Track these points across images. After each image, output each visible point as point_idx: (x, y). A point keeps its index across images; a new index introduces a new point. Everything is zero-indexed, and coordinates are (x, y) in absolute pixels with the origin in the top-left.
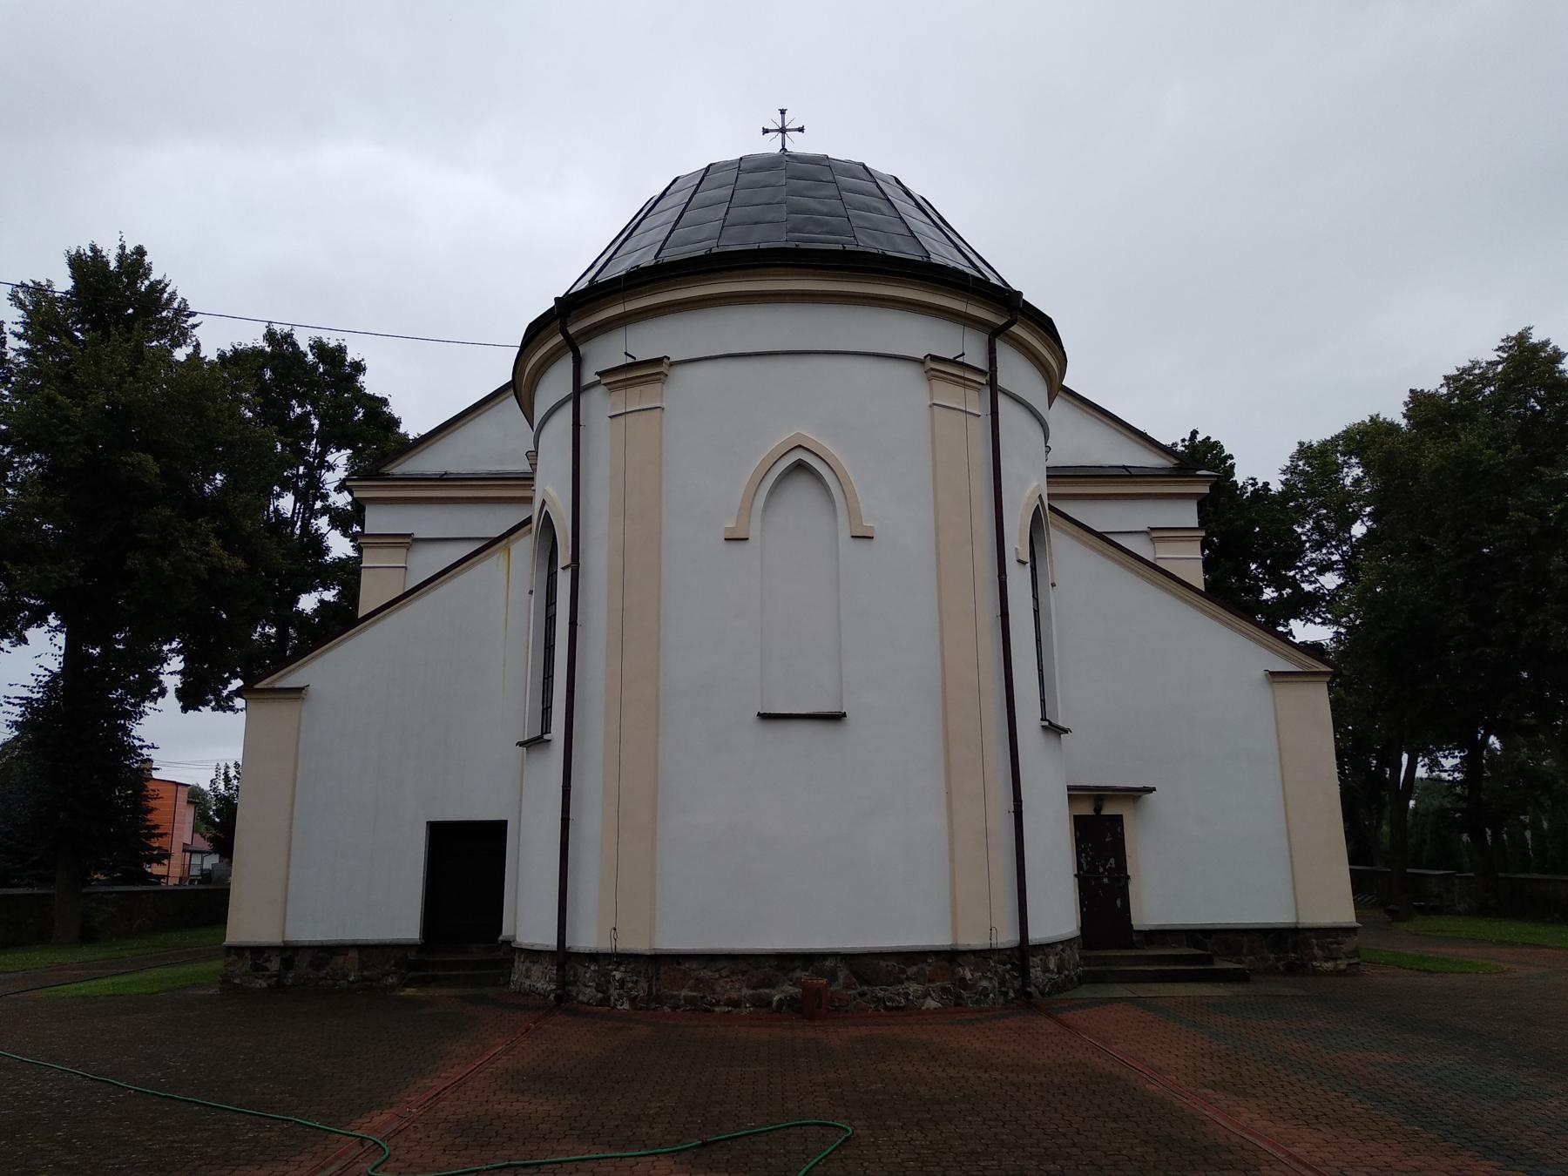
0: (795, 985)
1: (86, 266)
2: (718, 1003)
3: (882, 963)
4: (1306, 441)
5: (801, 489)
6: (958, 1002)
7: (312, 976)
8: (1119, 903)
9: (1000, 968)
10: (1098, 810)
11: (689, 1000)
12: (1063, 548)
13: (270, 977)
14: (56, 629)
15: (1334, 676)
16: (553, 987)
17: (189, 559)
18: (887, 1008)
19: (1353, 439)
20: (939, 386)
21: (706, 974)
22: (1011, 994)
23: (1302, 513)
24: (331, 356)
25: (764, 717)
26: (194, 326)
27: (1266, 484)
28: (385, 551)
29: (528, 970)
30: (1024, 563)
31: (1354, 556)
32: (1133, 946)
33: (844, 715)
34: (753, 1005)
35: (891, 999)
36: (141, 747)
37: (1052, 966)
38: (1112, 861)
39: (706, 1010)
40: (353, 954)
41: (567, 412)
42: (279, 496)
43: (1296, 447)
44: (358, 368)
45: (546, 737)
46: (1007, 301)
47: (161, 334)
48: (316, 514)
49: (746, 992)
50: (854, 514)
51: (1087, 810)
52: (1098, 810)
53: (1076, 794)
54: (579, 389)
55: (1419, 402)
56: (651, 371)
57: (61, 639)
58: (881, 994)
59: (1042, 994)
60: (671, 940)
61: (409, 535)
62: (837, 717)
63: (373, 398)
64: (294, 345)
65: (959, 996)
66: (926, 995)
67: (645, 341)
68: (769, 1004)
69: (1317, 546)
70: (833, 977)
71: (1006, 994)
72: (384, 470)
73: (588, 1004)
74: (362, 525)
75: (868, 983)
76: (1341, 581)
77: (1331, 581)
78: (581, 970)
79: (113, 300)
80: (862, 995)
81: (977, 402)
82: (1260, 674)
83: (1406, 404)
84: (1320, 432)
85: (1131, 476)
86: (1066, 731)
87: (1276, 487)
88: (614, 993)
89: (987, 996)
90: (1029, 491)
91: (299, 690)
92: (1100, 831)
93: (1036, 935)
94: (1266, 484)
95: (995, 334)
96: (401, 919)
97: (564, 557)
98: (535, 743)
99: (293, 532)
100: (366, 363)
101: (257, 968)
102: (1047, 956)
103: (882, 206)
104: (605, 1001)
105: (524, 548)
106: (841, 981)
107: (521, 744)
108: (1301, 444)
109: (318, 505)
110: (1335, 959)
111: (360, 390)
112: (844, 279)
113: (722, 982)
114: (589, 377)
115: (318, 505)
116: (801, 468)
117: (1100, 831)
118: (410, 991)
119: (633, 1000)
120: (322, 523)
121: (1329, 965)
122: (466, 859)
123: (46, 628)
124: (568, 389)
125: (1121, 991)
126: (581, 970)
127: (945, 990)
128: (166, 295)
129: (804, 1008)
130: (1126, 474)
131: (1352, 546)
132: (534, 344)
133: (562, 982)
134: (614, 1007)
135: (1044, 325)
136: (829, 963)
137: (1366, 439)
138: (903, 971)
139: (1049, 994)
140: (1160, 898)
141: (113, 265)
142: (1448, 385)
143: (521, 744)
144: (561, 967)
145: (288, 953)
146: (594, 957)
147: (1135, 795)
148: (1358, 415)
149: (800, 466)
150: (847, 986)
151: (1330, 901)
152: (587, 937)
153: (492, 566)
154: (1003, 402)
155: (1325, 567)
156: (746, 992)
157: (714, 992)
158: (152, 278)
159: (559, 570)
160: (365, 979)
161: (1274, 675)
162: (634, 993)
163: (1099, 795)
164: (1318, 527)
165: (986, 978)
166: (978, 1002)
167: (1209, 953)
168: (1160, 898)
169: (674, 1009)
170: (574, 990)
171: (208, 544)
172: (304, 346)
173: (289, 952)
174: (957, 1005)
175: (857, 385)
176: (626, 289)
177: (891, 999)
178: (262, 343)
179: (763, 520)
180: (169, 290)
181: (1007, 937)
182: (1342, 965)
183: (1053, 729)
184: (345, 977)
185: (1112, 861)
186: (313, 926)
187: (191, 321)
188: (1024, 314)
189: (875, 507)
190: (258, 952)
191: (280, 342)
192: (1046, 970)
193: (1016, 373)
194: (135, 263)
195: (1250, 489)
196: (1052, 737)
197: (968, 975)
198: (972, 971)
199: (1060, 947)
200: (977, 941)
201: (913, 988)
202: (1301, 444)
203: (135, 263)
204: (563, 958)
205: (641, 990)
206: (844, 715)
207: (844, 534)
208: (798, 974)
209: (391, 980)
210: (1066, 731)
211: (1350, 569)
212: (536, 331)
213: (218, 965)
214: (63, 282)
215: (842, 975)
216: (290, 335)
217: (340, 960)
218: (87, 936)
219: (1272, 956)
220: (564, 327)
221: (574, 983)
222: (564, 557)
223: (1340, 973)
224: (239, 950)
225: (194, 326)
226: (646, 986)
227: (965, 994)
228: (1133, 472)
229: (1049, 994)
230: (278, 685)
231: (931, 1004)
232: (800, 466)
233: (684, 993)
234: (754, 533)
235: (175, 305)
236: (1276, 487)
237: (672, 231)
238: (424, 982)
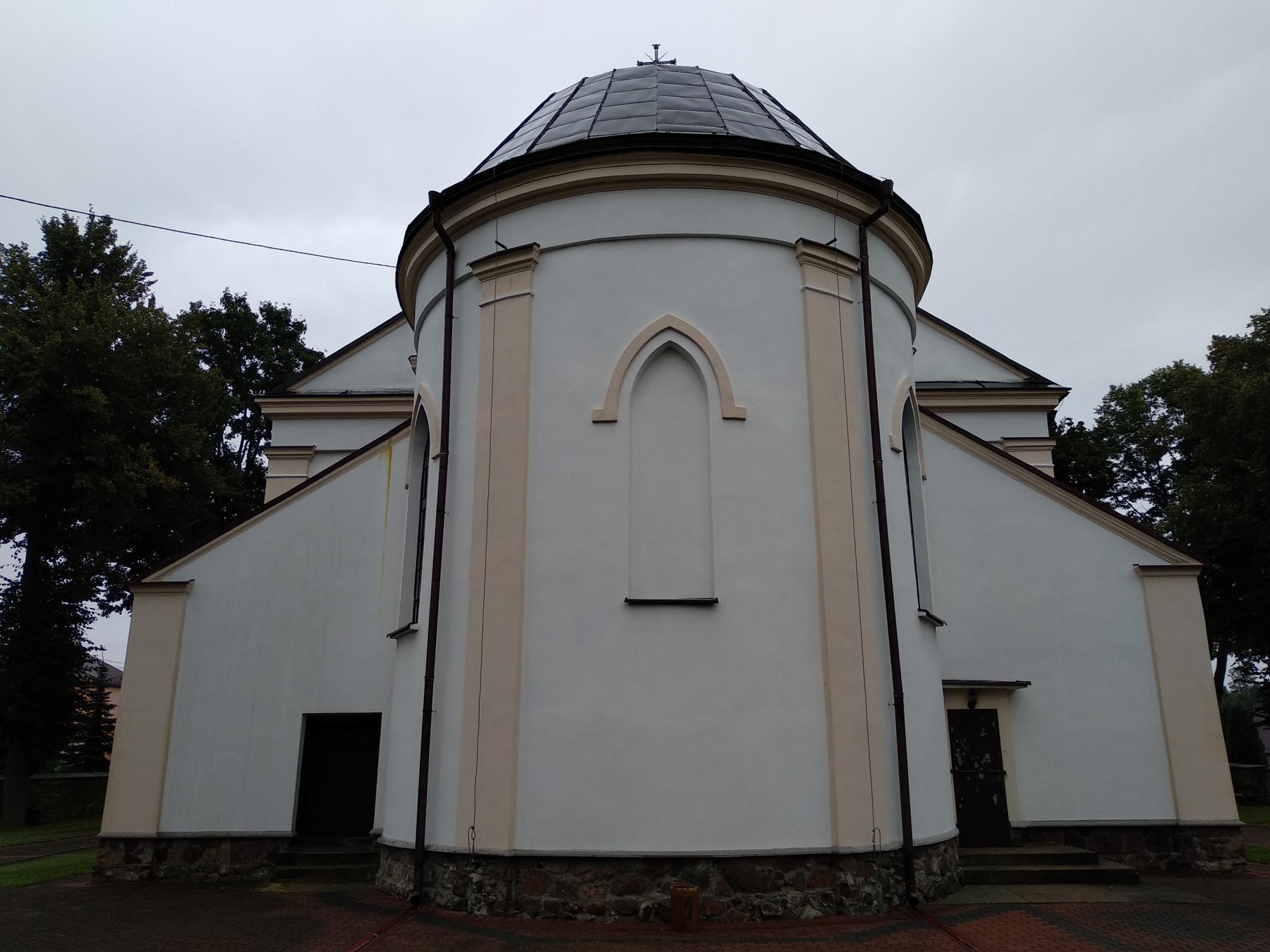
0: (663, 891)
1: (59, 233)
2: (580, 911)
3: (758, 868)
4: (1117, 385)
5: (671, 375)
6: (840, 909)
7: (186, 867)
8: (995, 798)
9: (884, 872)
10: (972, 704)
11: (549, 907)
12: (932, 443)
13: (143, 869)
14: (19, 545)
15: (1204, 571)
16: (411, 887)
17: (130, 479)
18: (764, 918)
19: (1158, 381)
20: (811, 270)
21: (568, 878)
22: (896, 901)
23: (1116, 449)
24: (277, 317)
25: (632, 603)
26: (151, 283)
27: (1081, 423)
28: (287, 462)
29: (390, 867)
30: (897, 451)
31: (1162, 485)
32: (1010, 844)
33: (716, 601)
34: (618, 913)
35: (767, 908)
36: (91, 648)
37: (935, 868)
38: (987, 756)
39: (571, 918)
40: (226, 847)
41: (441, 309)
42: (230, 436)
43: (1108, 390)
44: (300, 327)
45: (413, 627)
46: (879, 193)
47: (121, 290)
48: (259, 450)
49: (610, 898)
50: (725, 396)
51: (961, 704)
52: (972, 704)
53: (951, 688)
54: (452, 283)
55: (1222, 348)
56: (520, 258)
57: (23, 554)
58: (757, 902)
59: (926, 898)
60: (534, 840)
61: (311, 448)
62: (708, 604)
63: (311, 352)
64: (246, 307)
65: (840, 903)
66: (805, 902)
67: (514, 231)
68: (636, 912)
69: (1129, 476)
70: (704, 882)
71: (890, 900)
72: (290, 389)
73: (446, 907)
74: (268, 436)
75: (744, 890)
76: (1151, 506)
77: (1143, 506)
78: (439, 870)
79: (85, 259)
80: (736, 902)
81: (849, 289)
82: (1128, 568)
83: (1210, 348)
84: (1133, 373)
85: (985, 389)
86: (941, 623)
87: (1090, 425)
88: (471, 897)
89: (870, 903)
90: (900, 382)
91: (184, 584)
92: (975, 725)
93: (921, 835)
94: (1081, 423)
95: (865, 224)
96: (274, 811)
97: (435, 448)
98: (403, 634)
99: (240, 465)
100: (308, 323)
101: (130, 859)
102: (930, 858)
103: (753, 106)
104: (462, 905)
105: (403, 447)
106: (714, 886)
107: (392, 636)
108: (1113, 387)
109: (263, 442)
110: (1219, 859)
111: (302, 346)
112: (714, 163)
113: (585, 887)
114: (463, 269)
115: (263, 442)
116: (670, 351)
117: (975, 725)
118: (275, 887)
119: (491, 905)
120: (263, 459)
121: (1214, 865)
122: (339, 751)
123: (11, 543)
124: (442, 285)
125: (1007, 894)
126: (439, 870)
127: (826, 897)
128: (127, 257)
129: (674, 917)
130: (980, 388)
131: (1160, 477)
132: (412, 244)
133: (421, 883)
134: (471, 912)
135: (912, 220)
136: (700, 868)
137: (1173, 382)
138: (781, 877)
139: (933, 898)
140: (1041, 791)
141: (82, 231)
142: (1255, 324)
143: (392, 636)
144: (419, 867)
145: (161, 846)
146: (452, 857)
147: (1008, 689)
148: (1165, 361)
149: (670, 350)
150: (721, 893)
151: (1212, 800)
152: (447, 835)
153: (372, 467)
154: (874, 292)
155: (1137, 494)
156: (610, 898)
157: (577, 898)
158: (118, 244)
159: (431, 460)
160: (237, 872)
161: (1143, 568)
162: (492, 897)
163: (973, 690)
164: (1129, 457)
165: (868, 883)
166: (861, 909)
167: (1089, 850)
168: (1041, 791)
169: (535, 915)
170: (432, 892)
171: (147, 467)
172: (255, 309)
173: (163, 844)
174: (839, 913)
175: (732, 275)
176: (498, 179)
177: (767, 908)
178: (219, 306)
179: (632, 403)
180: (130, 253)
181: (890, 839)
182: (1227, 864)
183: (930, 620)
184: (217, 870)
185: (987, 756)
186: (185, 819)
187: (148, 279)
188: (894, 206)
189: (746, 387)
190: (131, 843)
191: (235, 305)
192: (930, 873)
193: (884, 265)
194: (102, 230)
195: (1067, 428)
196: (928, 629)
197: (851, 881)
198: (855, 876)
199: (942, 847)
200: (855, 841)
201: (792, 895)
202: (1113, 387)
203: (102, 230)
204: (422, 856)
205: (499, 896)
206: (716, 601)
207: (716, 416)
208: (667, 879)
209: (260, 874)
210: (941, 623)
211: (1157, 494)
212: (414, 232)
213: (91, 857)
214: (37, 246)
215: (715, 879)
216: (243, 299)
217: (213, 852)
218: (33, 819)
219: (1153, 854)
220: (442, 225)
221: (432, 884)
222: (435, 448)
223: (1226, 874)
224: (113, 841)
225: (151, 283)
226: (504, 890)
227: (847, 902)
228: (986, 386)
229: (933, 898)
230: (165, 579)
231: (811, 912)
232: (670, 350)
233: (545, 898)
234: (623, 416)
235: (135, 265)
236: (1090, 425)
237: (543, 132)
238: (291, 877)
